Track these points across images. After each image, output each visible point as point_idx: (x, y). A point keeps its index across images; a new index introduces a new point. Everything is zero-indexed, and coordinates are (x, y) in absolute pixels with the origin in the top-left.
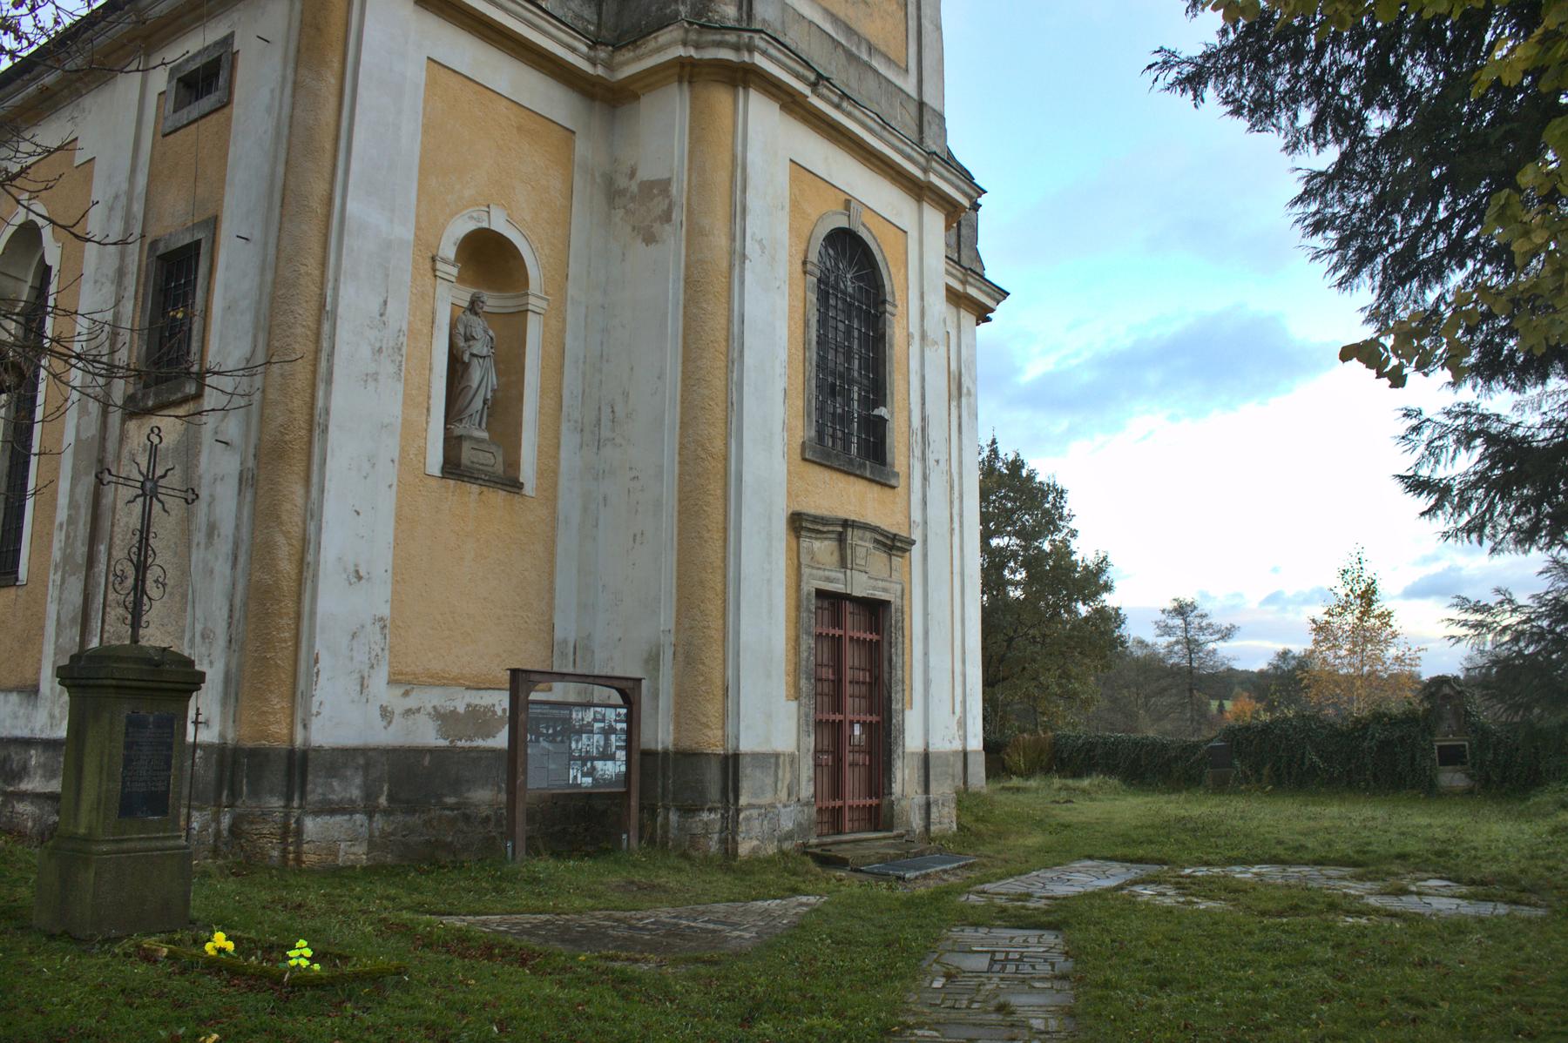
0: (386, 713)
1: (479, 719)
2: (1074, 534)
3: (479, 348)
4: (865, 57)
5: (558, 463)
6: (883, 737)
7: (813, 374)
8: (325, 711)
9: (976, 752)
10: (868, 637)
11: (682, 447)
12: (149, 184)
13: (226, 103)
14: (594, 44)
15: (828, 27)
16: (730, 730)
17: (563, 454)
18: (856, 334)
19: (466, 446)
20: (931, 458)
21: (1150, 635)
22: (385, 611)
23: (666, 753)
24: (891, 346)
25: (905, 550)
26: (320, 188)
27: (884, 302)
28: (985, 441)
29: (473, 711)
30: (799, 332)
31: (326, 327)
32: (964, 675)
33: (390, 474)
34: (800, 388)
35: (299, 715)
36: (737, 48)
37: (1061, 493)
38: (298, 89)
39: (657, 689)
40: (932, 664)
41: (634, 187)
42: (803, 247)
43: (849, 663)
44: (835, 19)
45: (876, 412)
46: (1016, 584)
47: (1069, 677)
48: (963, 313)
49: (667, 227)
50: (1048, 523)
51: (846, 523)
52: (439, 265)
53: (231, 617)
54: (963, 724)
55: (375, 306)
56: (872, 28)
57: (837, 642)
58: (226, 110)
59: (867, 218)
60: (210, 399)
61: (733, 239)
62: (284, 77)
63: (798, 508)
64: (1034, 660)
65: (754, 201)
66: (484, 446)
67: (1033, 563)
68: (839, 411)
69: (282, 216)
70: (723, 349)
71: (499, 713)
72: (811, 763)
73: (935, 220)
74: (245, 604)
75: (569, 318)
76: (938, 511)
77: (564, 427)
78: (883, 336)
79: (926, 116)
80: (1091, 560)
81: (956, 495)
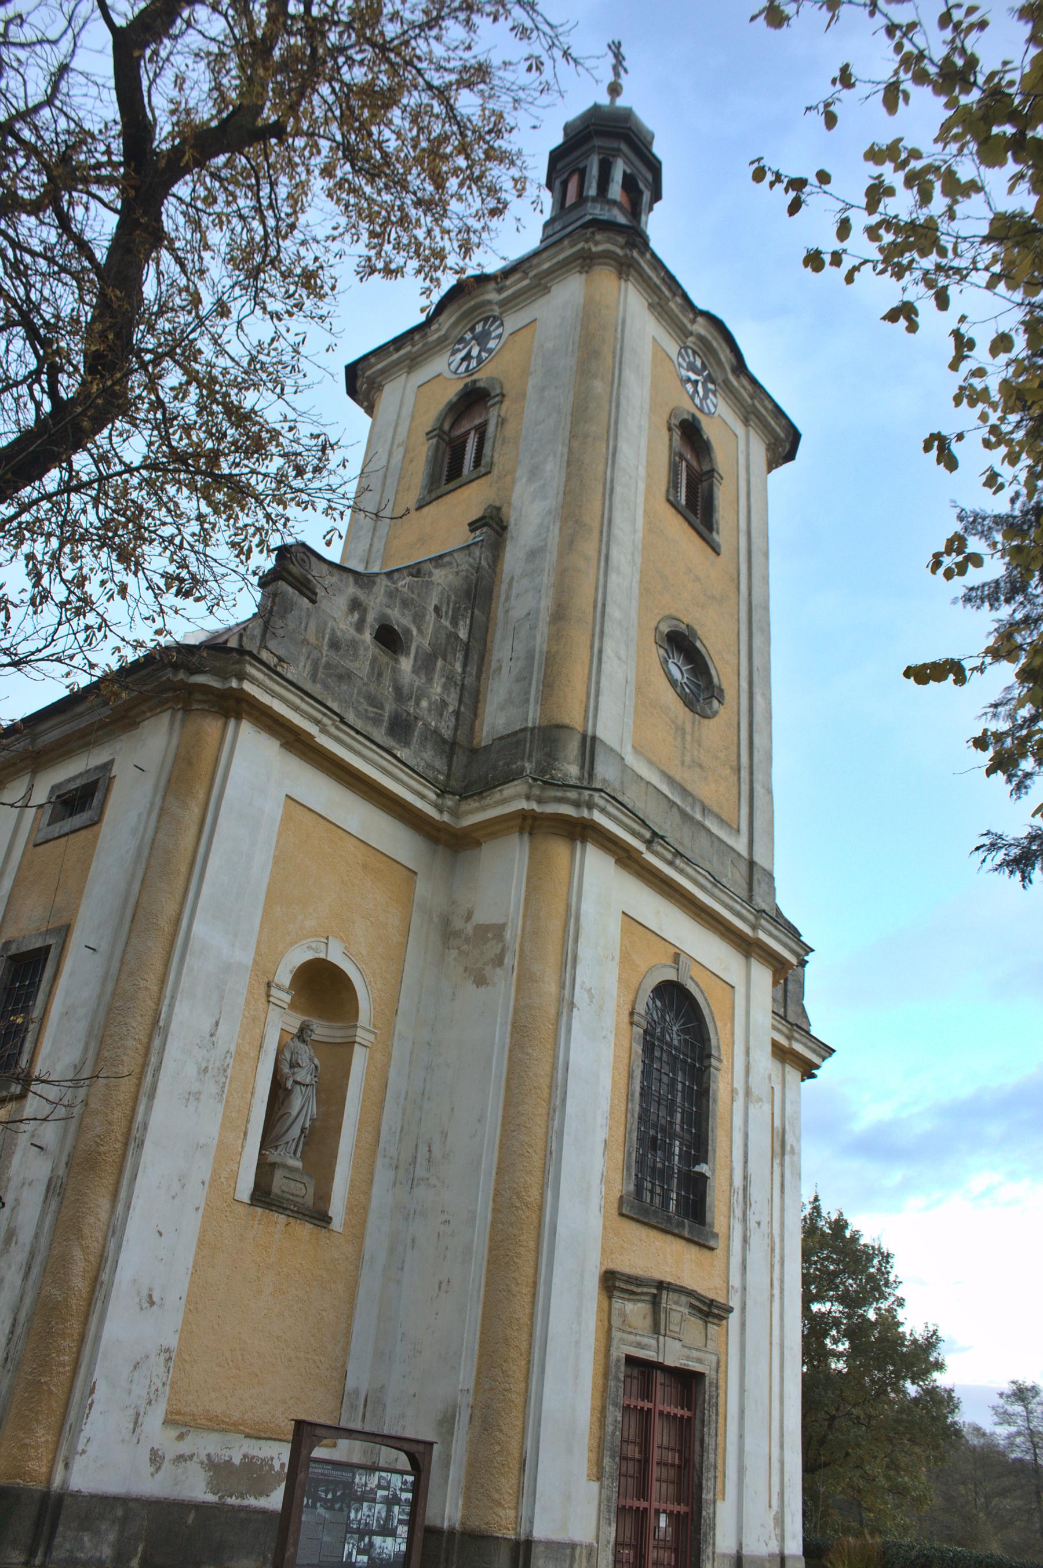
0: (156, 1458)
1: (254, 1473)
2: (900, 1302)
3: (303, 1075)
4: (698, 816)
5: (369, 1199)
7: (635, 1127)
8: (92, 1450)
9: (794, 1557)
10: (679, 1412)
11: (497, 1193)
12: (13, 889)
13: (96, 822)
14: (442, 793)
15: (665, 789)
16: (524, 1512)
17: (376, 1191)
18: (680, 1087)
19: (278, 1174)
20: (752, 1219)
21: (987, 1423)
22: (173, 1341)
23: (452, 1532)
24: (715, 1101)
25: (722, 1318)
26: (170, 908)
27: (709, 1056)
28: (807, 1197)
29: (249, 1462)
31: (157, 1042)
32: (782, 1462)
33: (197, 1194)
34: (621, 1140)
35: (63, 1452)
36: (577, 804)
37: (886, 1257)
38: (164, 815)
39: (449, 1456)
40: (747, 1448)
41: (469, 929)
42: (631, 997)
43: (657, 1441)
44: (671, 781)
45: (697, 1169)
46: (838, 1356)
47: (897, 1469)
48: (788, 1068)
49: (498, 970)
50: (873, 1289)
51: (661, 1285)
52: (274, 991)
53: (12, 1332)
54: (780, 1521)
55: (207, 1026)
56: (707, 790)
57: (645, 1416)
58: (95, 828)
59: (695, 971)
60: (32, 1106)
61: (562, 986)
62: (152, 804)
63: (612, 1266)
64: (858, 1445)
65: (585, 951)
66: (297, 1177)
67: (857, 1331)
68: (659, 1165)
69: (130, 931)
70: (546, 1095)
71: (277, 1468)
72: (611, 1558)
73: (762, 976)
74: (30, 1320)
75: (395, 1053)
76: (758, 1277)
77: (379, 1162)
78: (707, 1091)
79: (756, 876)
80: (920, 1334)
81: (777, 1258)
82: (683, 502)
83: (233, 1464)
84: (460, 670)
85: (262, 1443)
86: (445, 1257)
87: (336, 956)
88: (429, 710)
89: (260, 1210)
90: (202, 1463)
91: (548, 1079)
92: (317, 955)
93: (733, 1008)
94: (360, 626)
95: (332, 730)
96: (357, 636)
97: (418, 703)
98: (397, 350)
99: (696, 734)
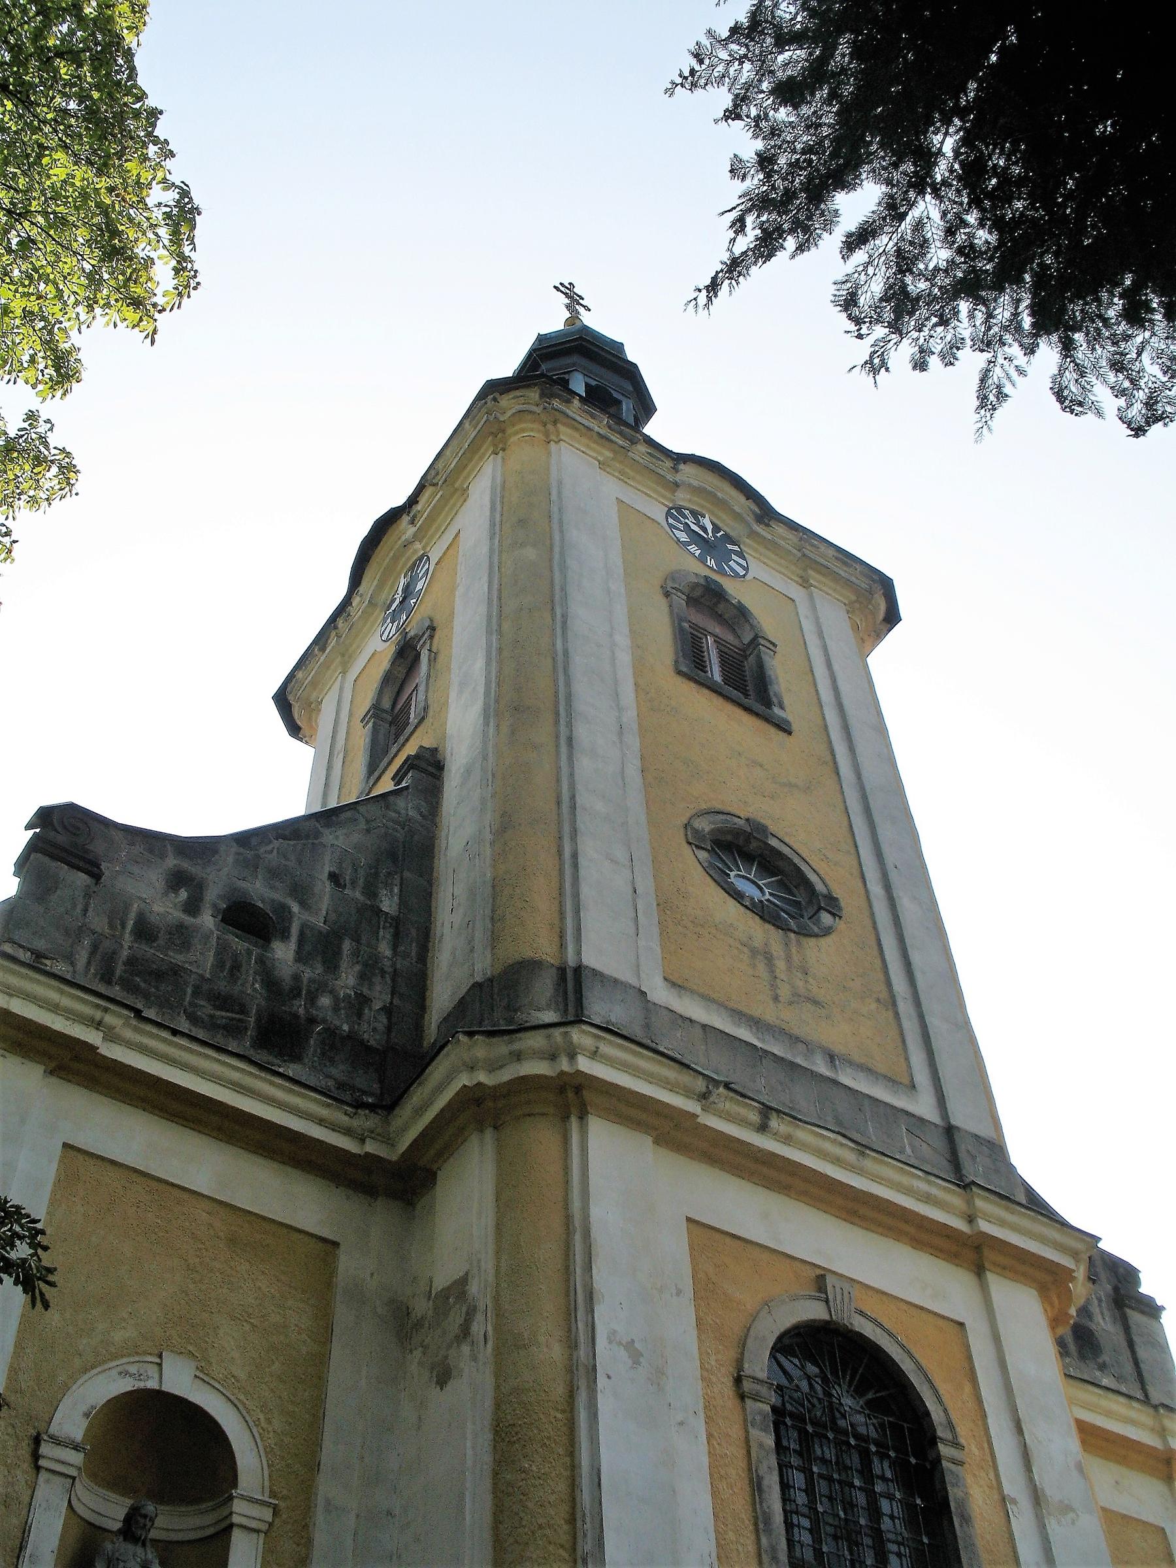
4: (822, 1068)
24: (966, 1520)
27: (933, 1440)
30: (740, 1503)
42: (732, 1354)
44: (738, 1015)
52: (45, 1449)
70: (564, 1538)
82: (717, 677)
84: (388, 953)
87: (179, 1379)
88: (336, 1009)
91: (565, 1508)
92: (141, 1385)
93: (970, 1358)
94: (193, 907)
95: (128, 1034)
96: (188, 920)
97: (312, 999)
98: (323, 649)
99: (796, 958)
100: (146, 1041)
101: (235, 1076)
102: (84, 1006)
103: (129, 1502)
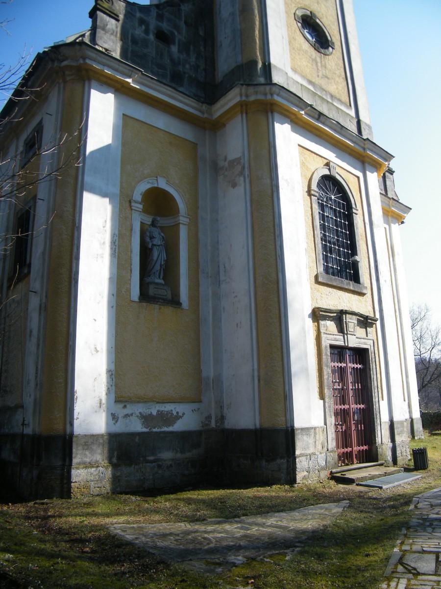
3: (157, 241)
4: (330, 100)
6: (368, 417)
15: (305, 83)
19: (151, 287)
27: (351, 208)
29: (160, 414)
41: (226, 164)
44: (310, 82)
51: (342, 313)
52: (133, 204)
53: (37, 373)
83: (153, 415)
84: (203, 50)
85: (166, 405)
86: (237, 312)
87: (162, 184)
89: (145, 304)
90: (138, 416)
92: (153, 186)
94: (147, 32)
96: (146, 37)
99: (323, 63)
100: (176, 96)
101: (169, 93)
102: (169, 91)
103: (153, 217)
